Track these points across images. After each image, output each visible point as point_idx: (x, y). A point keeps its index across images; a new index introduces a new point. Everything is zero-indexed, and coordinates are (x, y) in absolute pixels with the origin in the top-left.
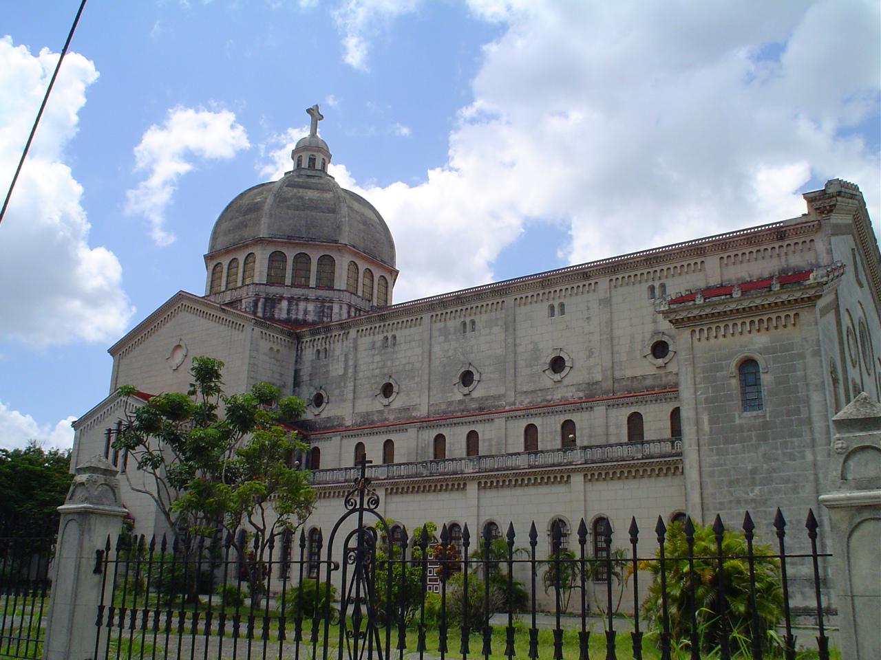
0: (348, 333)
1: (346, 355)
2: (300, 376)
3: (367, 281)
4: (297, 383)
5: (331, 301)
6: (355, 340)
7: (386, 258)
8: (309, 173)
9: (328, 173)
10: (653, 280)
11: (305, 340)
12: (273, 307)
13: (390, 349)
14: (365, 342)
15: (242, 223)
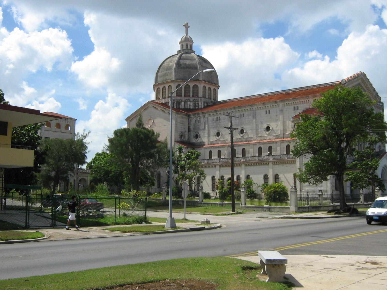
0: (205, 115)
1: (205, 122)
2: (190, 128)
3: (209, 92)
4: (189, 130)
5: (198, 101)
6: (207, 118)
7: (215, 82)
8: (187, 51)
9: (193, 50)
10: (295, 105)
11: (191, 117)
12: (179, 104)
13: (218, 121)
14: (210, 118)
15: (166, 74)
